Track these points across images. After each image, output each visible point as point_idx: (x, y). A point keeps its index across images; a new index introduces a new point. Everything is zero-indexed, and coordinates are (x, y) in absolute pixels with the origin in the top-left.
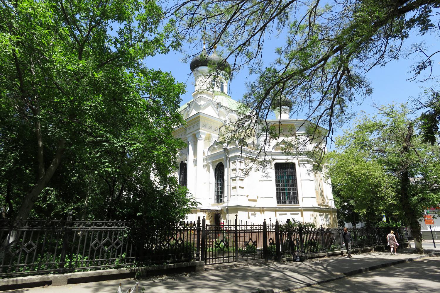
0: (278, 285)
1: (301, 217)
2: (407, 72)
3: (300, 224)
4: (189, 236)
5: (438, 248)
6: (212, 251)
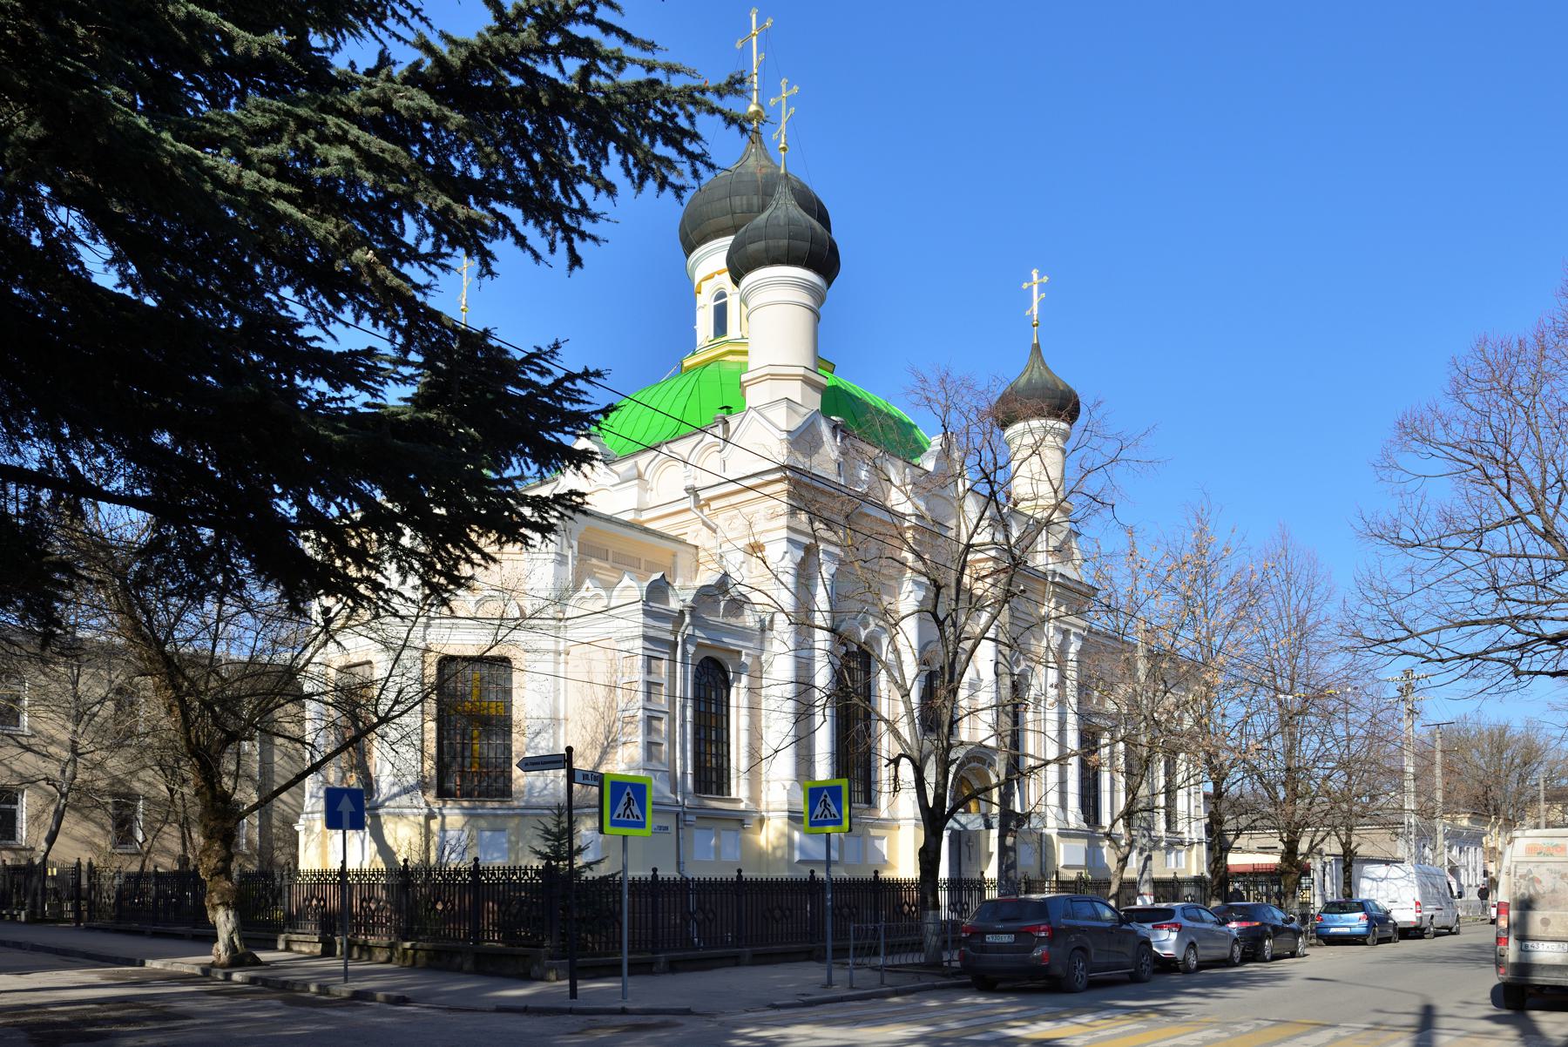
0: (601, 568)
1: (537, 263)
2: (1377, 478)
3: (918, 665)
4: (643, 920)
5: (1564, 665)
6: (1532, 590)
